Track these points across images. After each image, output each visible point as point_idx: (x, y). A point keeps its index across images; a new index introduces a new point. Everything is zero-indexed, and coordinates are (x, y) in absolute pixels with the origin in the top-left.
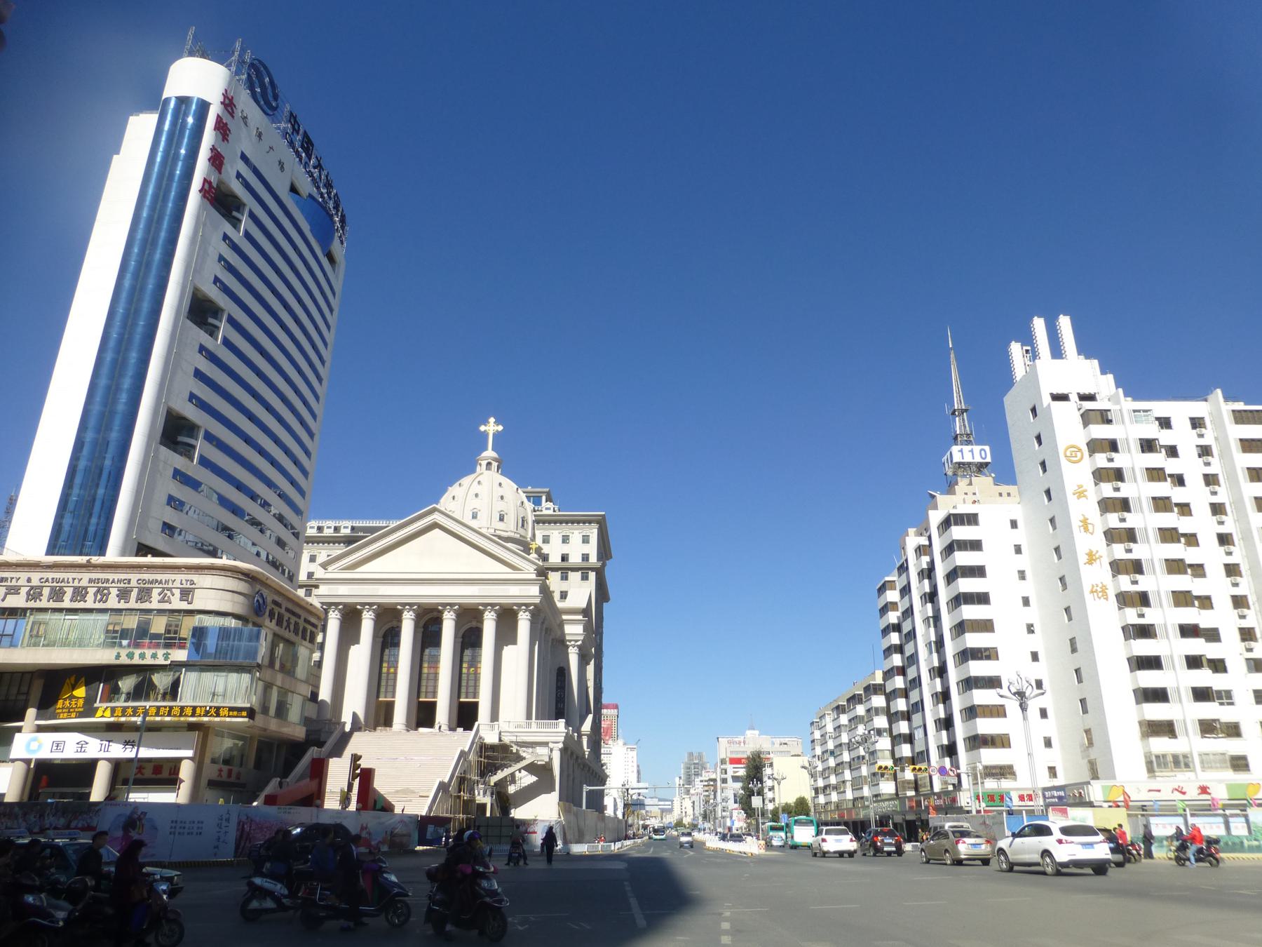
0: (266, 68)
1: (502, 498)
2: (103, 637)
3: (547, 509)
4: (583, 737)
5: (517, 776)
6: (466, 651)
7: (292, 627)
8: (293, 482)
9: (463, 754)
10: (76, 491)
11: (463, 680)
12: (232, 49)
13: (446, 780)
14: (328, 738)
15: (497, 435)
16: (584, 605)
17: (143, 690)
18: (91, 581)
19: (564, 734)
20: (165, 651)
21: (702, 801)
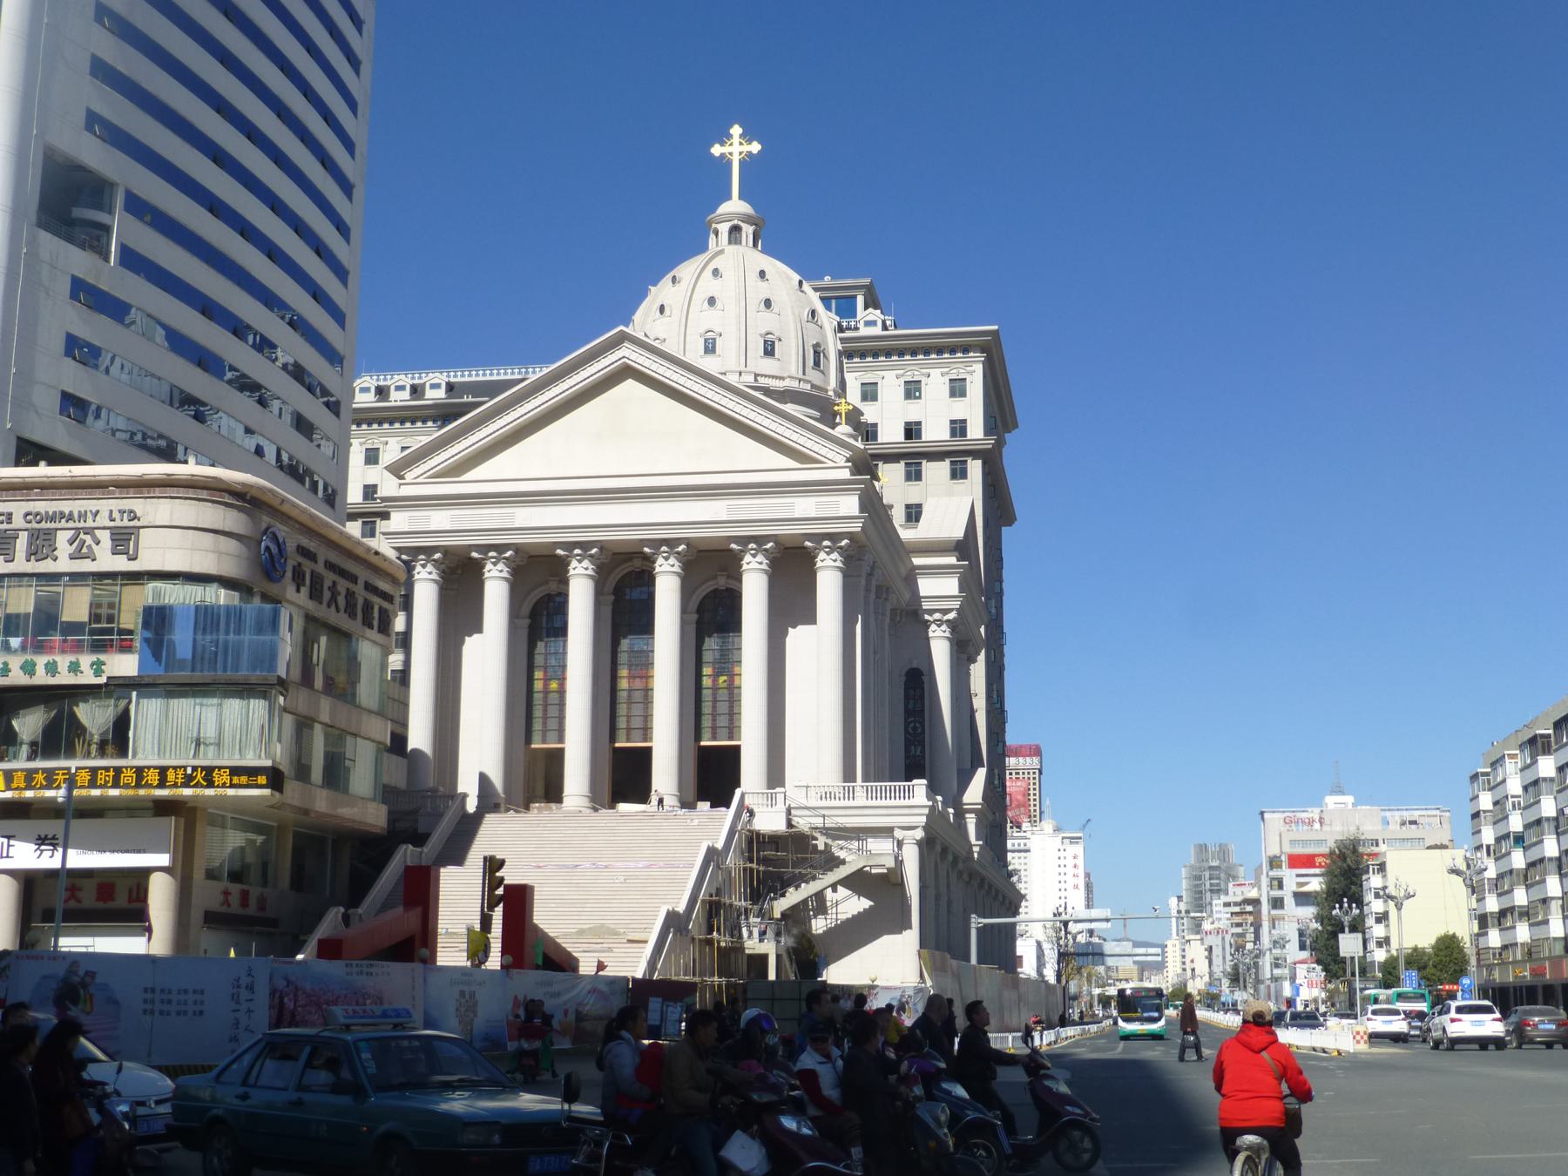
1: (768, 303)
3: (868, 324)
4: (967, 815)
7: (341, 600)
8: (318, 295)
9: (712, 854)
15: (748, 163)
16: (958, 532)
19: (926, 811)
20: (94, 658)
21: (1228, 946)
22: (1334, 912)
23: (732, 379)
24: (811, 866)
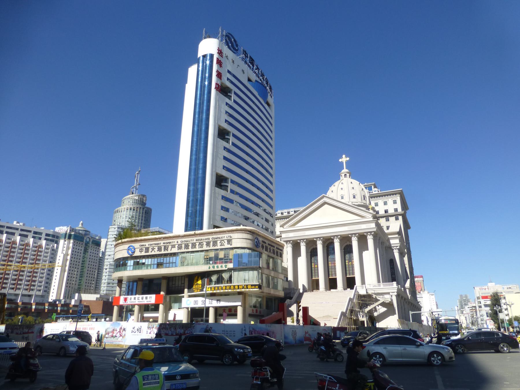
0: (231, 35)
1: (353, 188)
2: (204, 261)
3: (375, 191)
4: (407, 289)
5: (377, 308)
6: (346, 255)
7: (272, 251)
8: (267, 195)
9: (350, 300)
10: (190, 209)
11: (347, 268)
12: (218, 32)
13: (344, 311)
14: (294, 295)
15: (347, 162)
16: (398, 230)
17: (220, 280)
18: (196, 240)
19: (397, 289)
20: (225, 264)
21: (470, 317)
22: (494, 308)
23: (348, 203)
24: (372, 301)
